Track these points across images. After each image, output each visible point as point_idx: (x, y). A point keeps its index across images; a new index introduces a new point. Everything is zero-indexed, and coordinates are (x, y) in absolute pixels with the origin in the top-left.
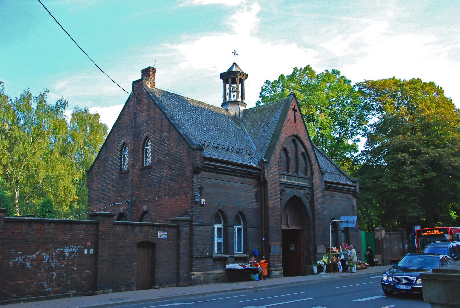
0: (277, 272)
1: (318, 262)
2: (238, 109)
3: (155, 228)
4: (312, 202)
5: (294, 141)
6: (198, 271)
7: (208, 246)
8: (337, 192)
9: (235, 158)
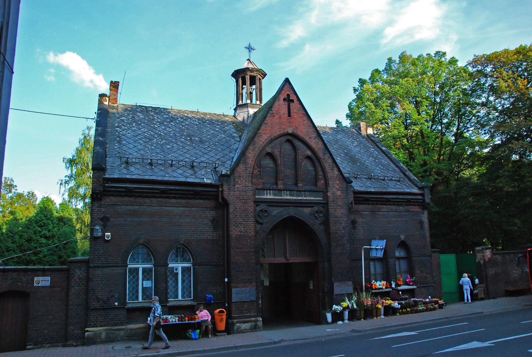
0: (246, 324)
1: (335, 307)
2: (247, 113)
3: (30, 273)
4: (326, 223)
5: (288, 141)
6: (97, 327)
7: (117, 293)
8: (386, 205)
9: (159, 175)
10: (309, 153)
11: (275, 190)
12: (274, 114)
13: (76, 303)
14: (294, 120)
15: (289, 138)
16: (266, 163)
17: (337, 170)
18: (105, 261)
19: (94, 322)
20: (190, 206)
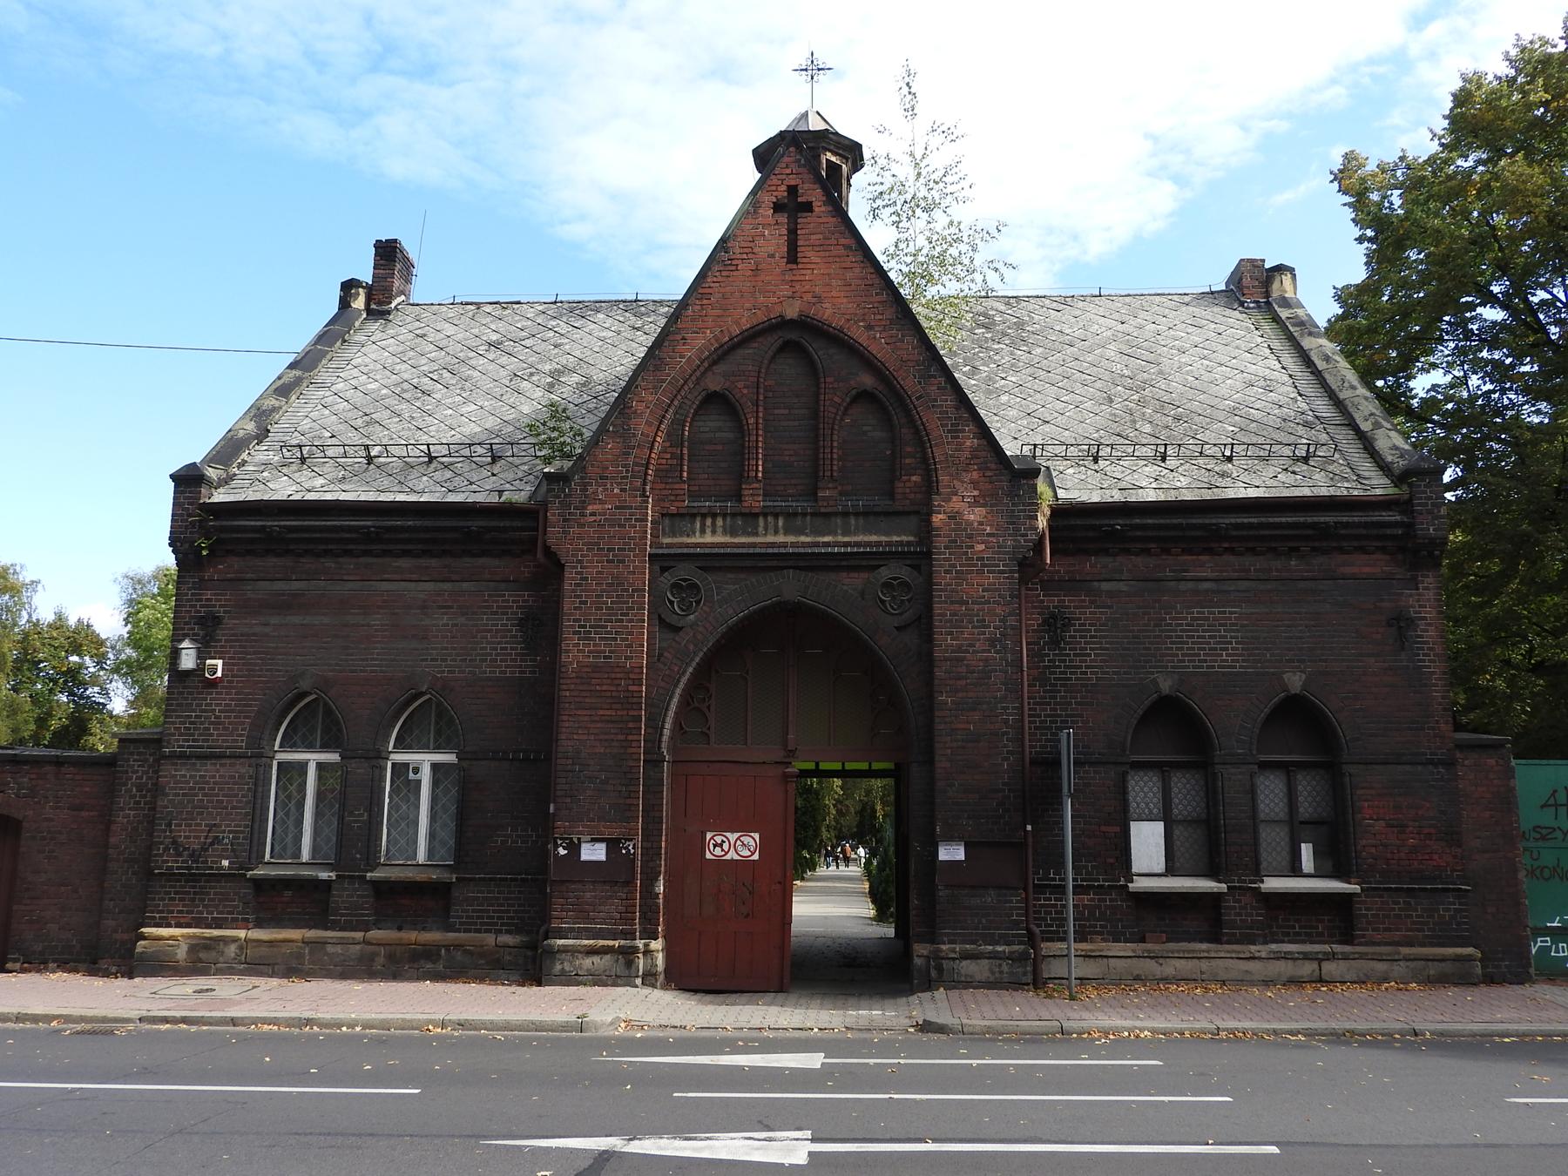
4: (923, 623)
5: (787, 347)
6: (169, 926)
7: (230, 832)
10: (867, 381)
11: (734, 515)
12: (734, 262)
13: (126, 856)
14: (809, 272)
15: (792, 335)
16: (708, 429)
17: (976, 430)
18: (203, 741)
19: (162, 912)
20: (454, 577)
